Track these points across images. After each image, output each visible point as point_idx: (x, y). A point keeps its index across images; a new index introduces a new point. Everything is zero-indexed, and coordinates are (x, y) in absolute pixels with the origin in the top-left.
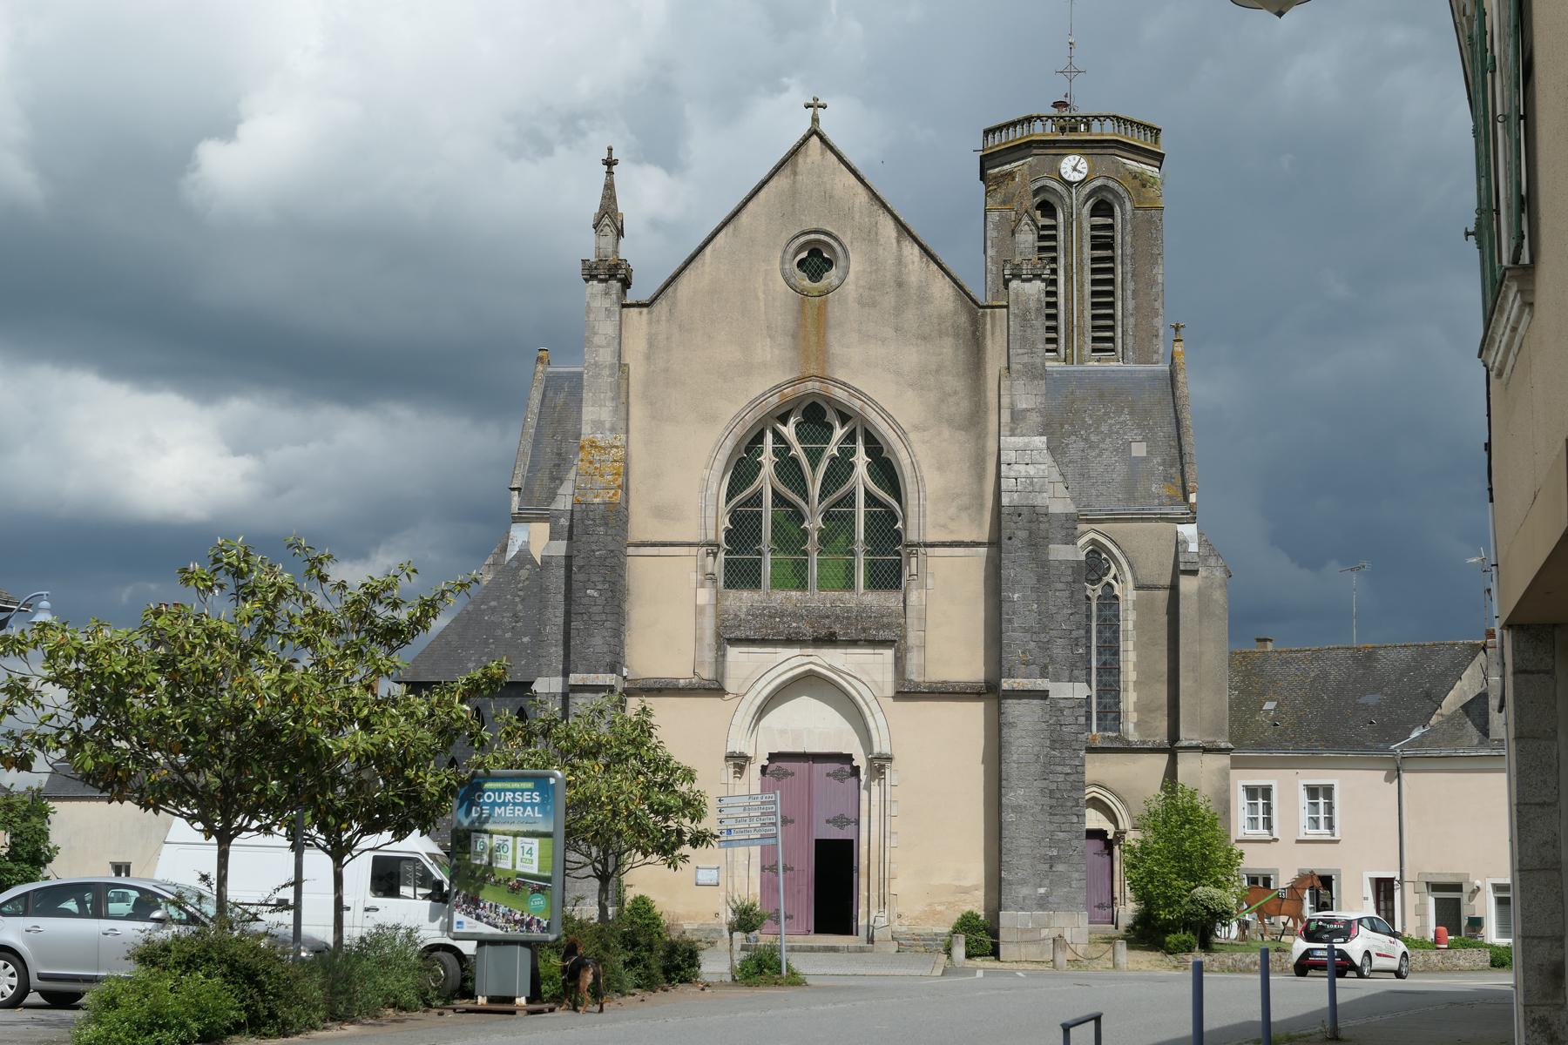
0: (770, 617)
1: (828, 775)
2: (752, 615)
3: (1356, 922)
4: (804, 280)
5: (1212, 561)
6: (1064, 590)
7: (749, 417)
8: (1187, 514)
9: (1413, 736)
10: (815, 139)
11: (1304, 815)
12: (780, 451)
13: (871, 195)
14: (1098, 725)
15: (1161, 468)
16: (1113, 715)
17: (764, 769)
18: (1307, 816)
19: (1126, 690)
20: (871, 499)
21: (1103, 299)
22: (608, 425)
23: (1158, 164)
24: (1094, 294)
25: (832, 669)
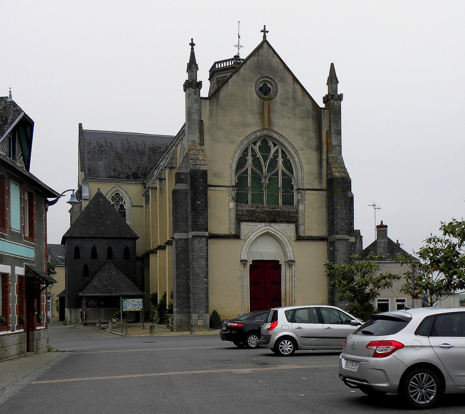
7: (245, 142)
20: (283, 173)
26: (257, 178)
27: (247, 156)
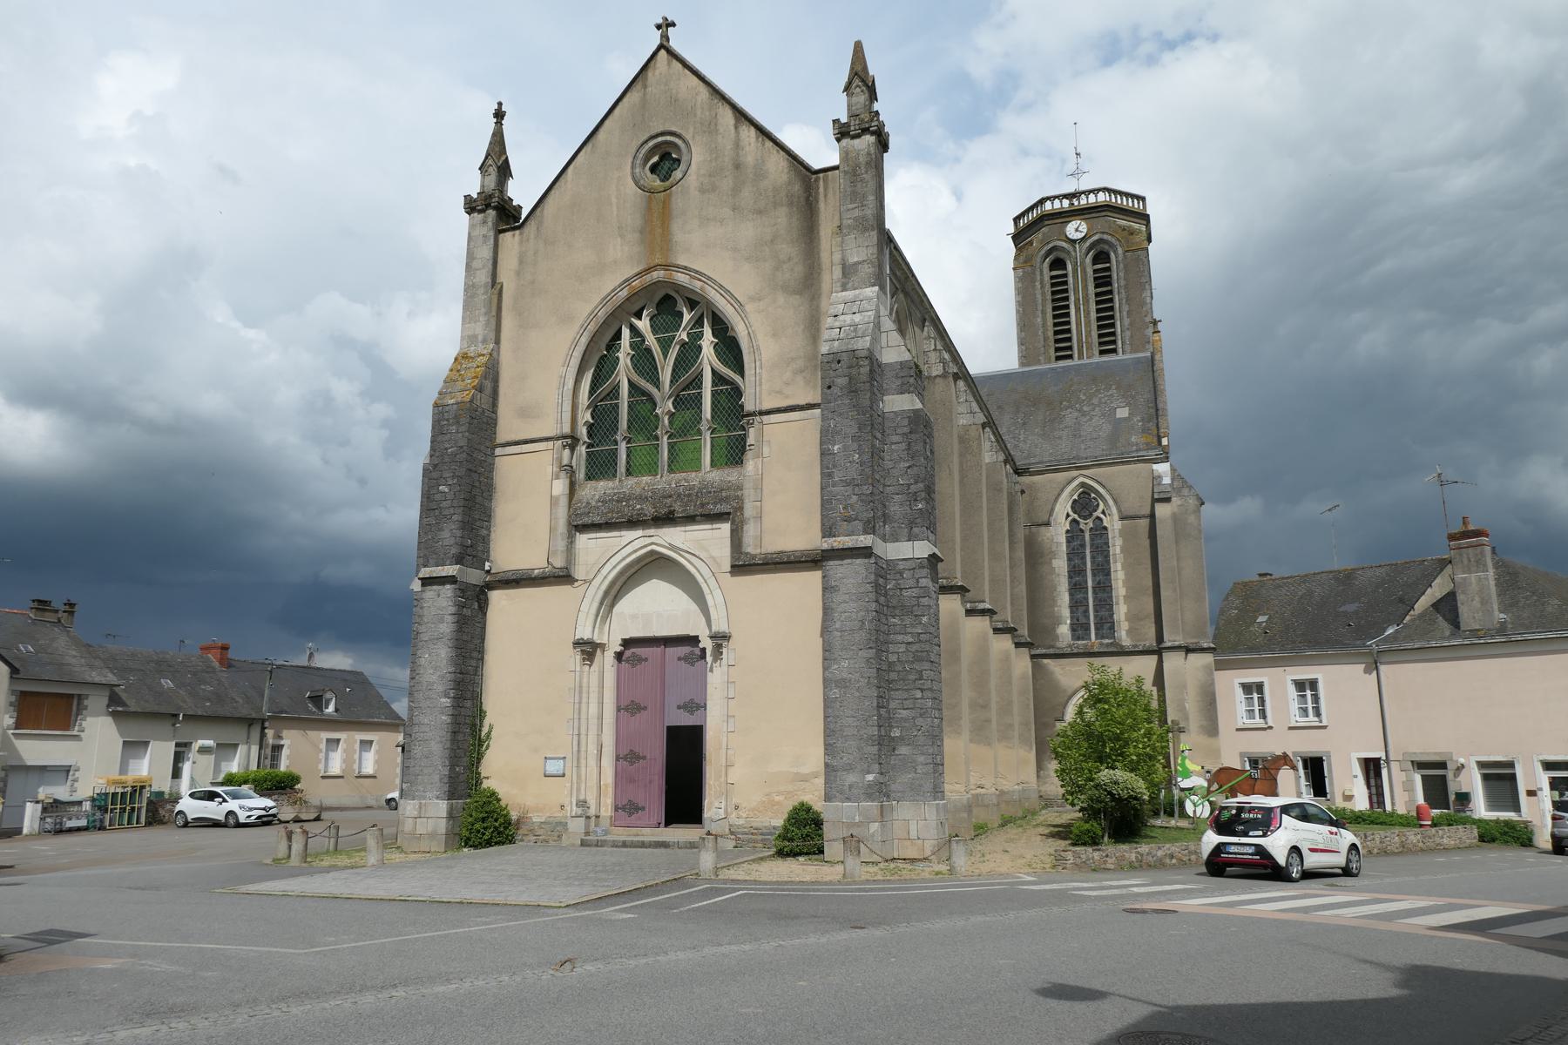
0: (618, 501)
1: (679, 659)
2: (602, 502)
3: (1279, 810)
4: (654, 181)
5: (1185, 492)
6: (899, 443)
8: (1161, 454)
9: (1386, 634)
10: (663, 52)
11: (1294, 706)
12: (636, 344)
13: (711, 90)
14: (1096, 634)
15: (1140, 424)
16: (1109, 624)
17: (619, 656)
18: (1297, 706)
19: (1117, 604)
20: (718, 378)
21: (1106, 321)
22: (480, 338)
23: (1145, 223)
24: (1099, 319)
25: (672, 547)
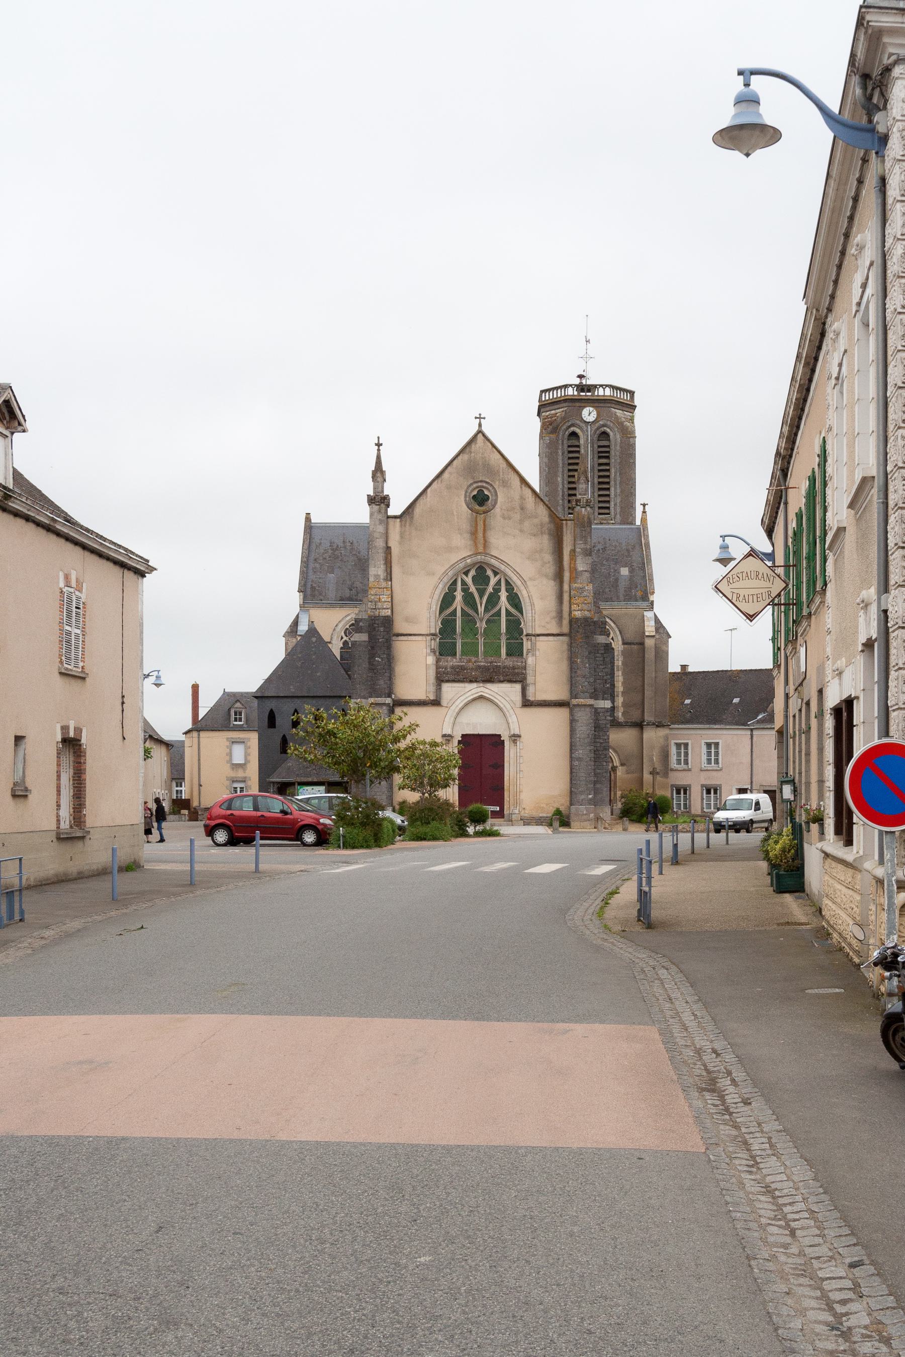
11: (704, 758)
19: (618, 696)
20: (508, 613)
21: (604, 485)
26: (469, 621)
27: (455, 591)
